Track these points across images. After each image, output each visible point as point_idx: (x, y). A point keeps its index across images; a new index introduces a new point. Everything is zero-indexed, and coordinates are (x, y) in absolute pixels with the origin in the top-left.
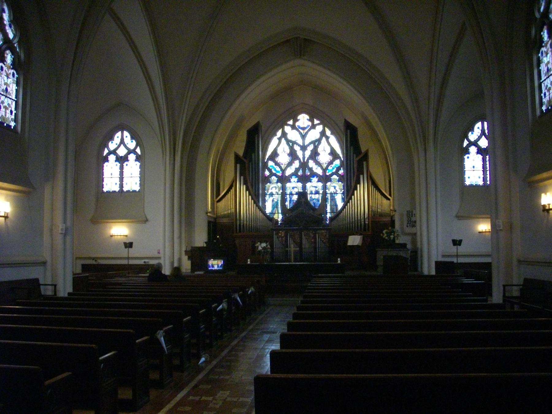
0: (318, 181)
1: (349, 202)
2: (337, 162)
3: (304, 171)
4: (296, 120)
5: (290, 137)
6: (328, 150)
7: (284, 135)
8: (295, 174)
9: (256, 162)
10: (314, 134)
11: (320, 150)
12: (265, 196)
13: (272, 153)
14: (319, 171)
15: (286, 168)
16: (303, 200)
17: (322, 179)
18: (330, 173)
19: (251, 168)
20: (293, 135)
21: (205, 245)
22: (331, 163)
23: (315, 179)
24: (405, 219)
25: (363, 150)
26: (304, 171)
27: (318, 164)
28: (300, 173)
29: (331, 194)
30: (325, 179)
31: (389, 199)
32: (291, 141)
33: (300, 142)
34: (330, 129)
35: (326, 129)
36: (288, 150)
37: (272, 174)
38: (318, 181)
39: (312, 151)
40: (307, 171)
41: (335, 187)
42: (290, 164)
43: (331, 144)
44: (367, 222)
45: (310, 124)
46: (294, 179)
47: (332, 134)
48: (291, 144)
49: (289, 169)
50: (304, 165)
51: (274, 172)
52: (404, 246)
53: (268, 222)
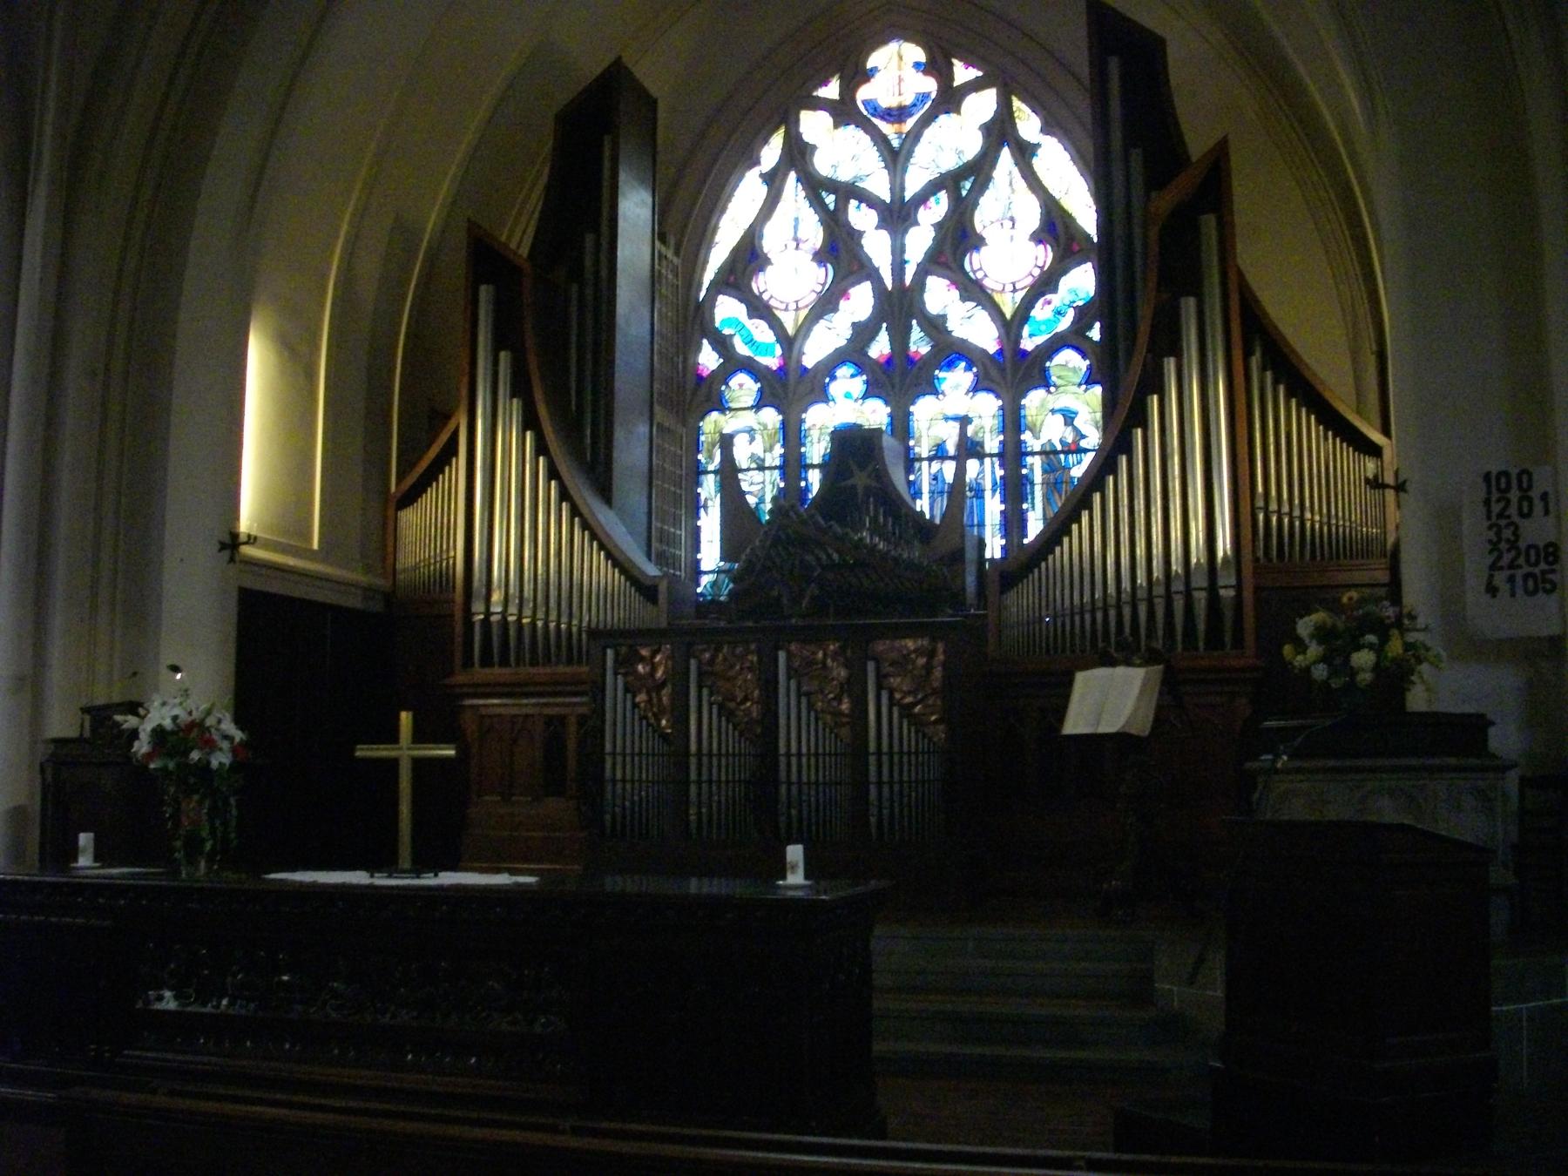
0: (976, 388)
1: (1114, 470)
2: (1081, 282)
3: (900, 338)
4: (857, 75)
5: (823, 164)
6: (1031, 215)
7: (798, 154)
8: (853, 353)
9: (604, 273)
10: (954, 139)
11: (984, 217)
12: (698, 484)
13: (736, 252)
14: (981, 332)
15: (806, 328)
16: (860, 480)
17: (994, 373)
18: (1040, 339)
19: (539, 306)
20: (840, 151)
22: (1046, 283)
23: (957, 380)
24: (1473, 527)
25: (1197, 144)
26: (900, 338)
27: (974, 291)
28: (880, 347)
29: (1048, 453)
30: (1012, 372)
31: (1375, 451)
32: (833, 186)
33: (880, 186)
34: (1037, 105)
35: (1017, 103)
36: (814, 234)
37: (733, 364)
38: (976, 388)
39: (938, 227)
40: (916, 333)
41: (1069, 417)
42: (827, 303)
43: (1046, 183)
44: (1227, 594)
45: (930, 85)
46: (847, 383)
47: (1046, 129)
48: (834, 199)
49: (820, 328)
50: (899, 306)
51: (742, 349)
52: (1466, 733)
53: (636, 599)
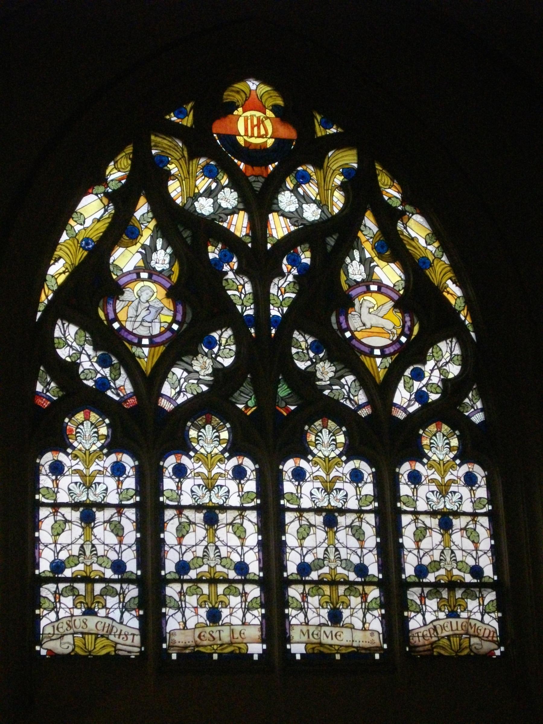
7: (149, 178)
20: (204, 192)
23: (326, 440)
48: (184, 229)
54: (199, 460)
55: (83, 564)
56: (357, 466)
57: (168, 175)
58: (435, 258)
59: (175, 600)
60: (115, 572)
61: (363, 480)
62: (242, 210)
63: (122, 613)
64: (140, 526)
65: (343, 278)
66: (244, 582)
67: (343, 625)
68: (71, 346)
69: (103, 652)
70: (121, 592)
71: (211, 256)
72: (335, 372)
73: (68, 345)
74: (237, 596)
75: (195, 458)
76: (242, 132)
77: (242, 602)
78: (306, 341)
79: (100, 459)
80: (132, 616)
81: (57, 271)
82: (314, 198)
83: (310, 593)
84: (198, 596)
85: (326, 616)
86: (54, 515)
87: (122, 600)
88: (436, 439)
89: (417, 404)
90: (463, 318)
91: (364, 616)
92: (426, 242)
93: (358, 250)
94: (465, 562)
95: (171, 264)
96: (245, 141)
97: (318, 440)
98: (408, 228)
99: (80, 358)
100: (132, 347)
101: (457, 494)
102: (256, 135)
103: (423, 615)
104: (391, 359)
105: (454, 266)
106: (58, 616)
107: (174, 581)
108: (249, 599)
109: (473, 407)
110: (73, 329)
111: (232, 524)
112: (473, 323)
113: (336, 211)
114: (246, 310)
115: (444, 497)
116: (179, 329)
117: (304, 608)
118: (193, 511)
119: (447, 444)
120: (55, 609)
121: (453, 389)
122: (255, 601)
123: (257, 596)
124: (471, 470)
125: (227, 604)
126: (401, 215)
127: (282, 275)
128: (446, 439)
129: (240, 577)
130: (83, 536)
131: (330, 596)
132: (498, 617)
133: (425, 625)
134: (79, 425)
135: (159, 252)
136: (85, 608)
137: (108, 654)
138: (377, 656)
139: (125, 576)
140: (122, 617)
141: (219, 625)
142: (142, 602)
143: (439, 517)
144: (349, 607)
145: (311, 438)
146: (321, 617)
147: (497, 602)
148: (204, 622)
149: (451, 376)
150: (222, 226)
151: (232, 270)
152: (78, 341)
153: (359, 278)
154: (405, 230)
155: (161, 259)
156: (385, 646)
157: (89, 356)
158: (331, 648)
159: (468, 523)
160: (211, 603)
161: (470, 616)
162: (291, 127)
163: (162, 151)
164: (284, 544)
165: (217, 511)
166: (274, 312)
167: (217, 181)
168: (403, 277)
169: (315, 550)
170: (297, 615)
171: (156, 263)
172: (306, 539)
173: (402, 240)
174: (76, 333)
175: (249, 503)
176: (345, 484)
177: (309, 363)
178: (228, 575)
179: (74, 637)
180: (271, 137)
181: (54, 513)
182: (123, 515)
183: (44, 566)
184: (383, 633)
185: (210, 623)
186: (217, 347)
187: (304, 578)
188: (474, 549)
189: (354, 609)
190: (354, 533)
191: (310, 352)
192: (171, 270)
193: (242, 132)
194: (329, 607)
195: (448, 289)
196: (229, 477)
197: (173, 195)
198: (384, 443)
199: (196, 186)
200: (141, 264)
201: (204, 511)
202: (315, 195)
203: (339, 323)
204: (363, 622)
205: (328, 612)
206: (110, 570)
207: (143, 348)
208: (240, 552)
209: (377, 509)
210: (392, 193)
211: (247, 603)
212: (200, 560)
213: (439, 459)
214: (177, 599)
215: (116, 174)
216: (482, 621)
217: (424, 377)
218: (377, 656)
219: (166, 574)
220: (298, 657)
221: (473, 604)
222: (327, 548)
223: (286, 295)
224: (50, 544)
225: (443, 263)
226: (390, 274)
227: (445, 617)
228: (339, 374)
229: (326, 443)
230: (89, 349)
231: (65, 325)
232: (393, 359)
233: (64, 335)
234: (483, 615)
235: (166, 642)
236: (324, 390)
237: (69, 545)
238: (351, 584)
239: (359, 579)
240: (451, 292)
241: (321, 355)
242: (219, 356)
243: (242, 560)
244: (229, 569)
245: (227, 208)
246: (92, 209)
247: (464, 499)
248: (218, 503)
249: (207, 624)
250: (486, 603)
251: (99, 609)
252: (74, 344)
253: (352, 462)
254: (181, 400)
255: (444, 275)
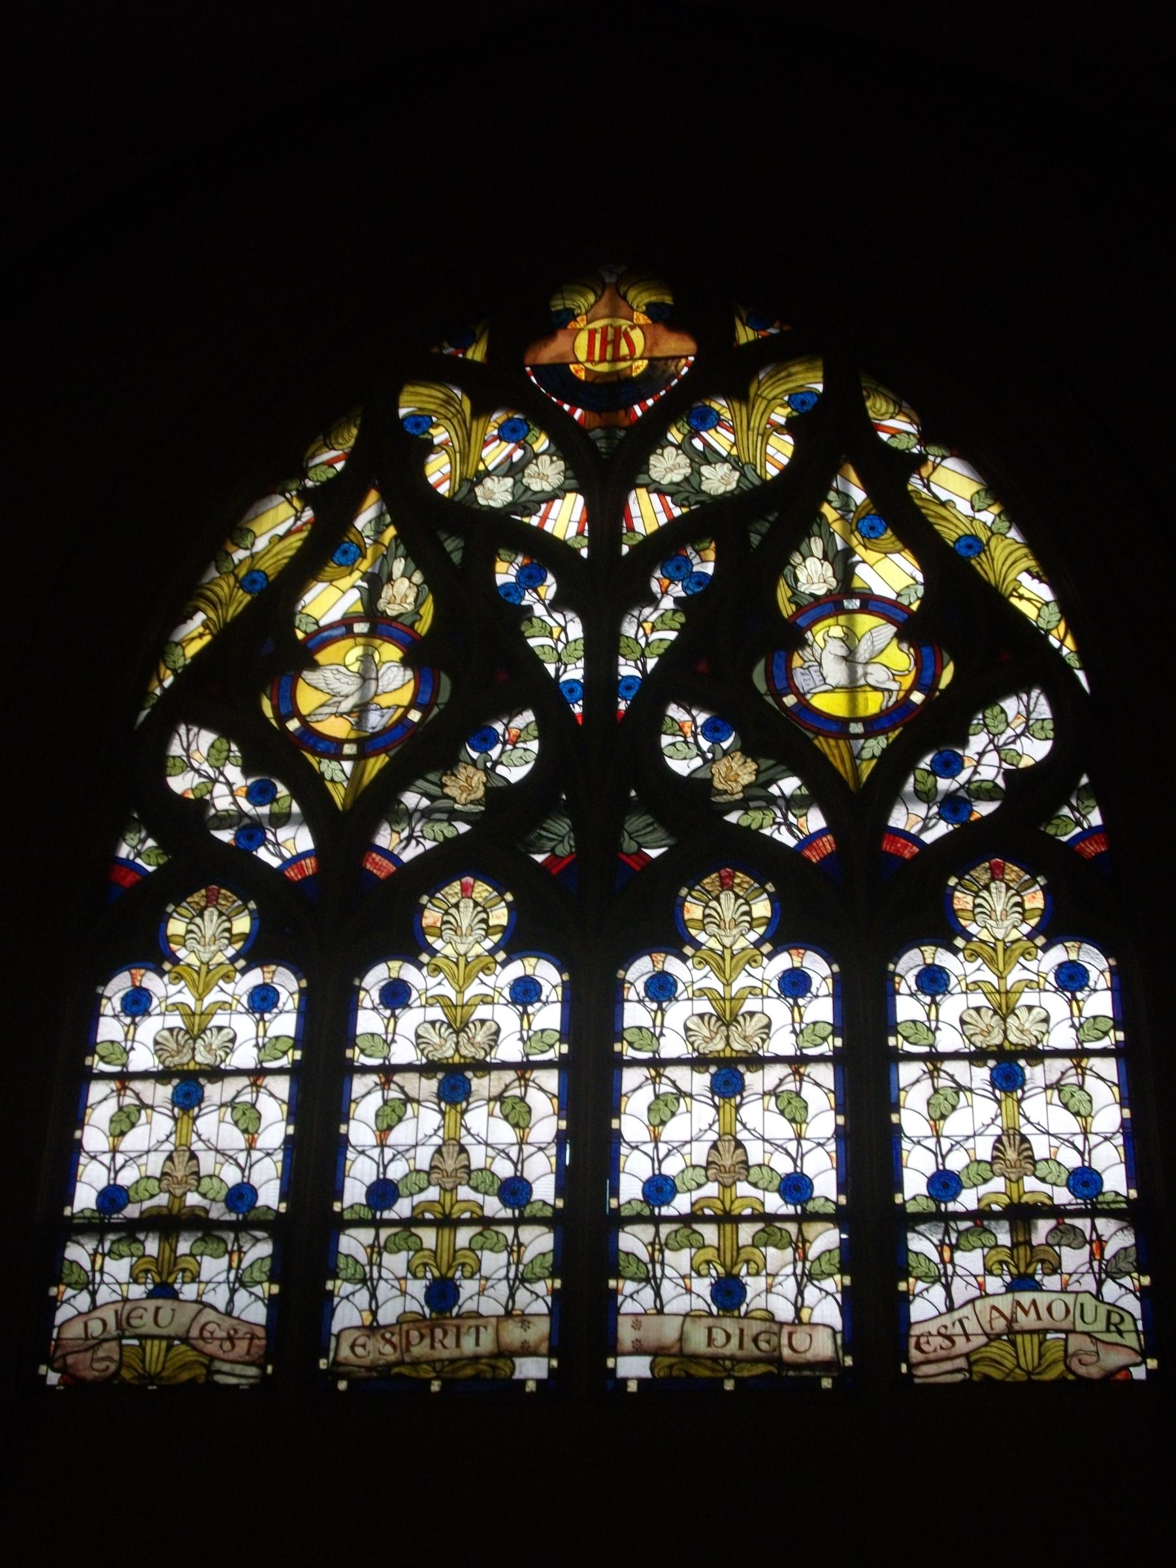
7: (392, 459)
8: (491, 845)
20: (479, 458)
21: (100, 990)
27: (784, 736)
48: (456, 540)
50: (600, 750)
54: (976, 955)
55: (438, 1188)
56: (529, 971)
57: (429, 447)
58: (993, 534)
59: (639, 1260)
60: (506, 1203)
61: (276, 1006)
62: (571, 491)
63: (233, 1292)
64: (296, 1111)
65: (783, 593)
66: (1093, 1213)
67: (747, 1313)
68: (197, 771)
69: (185, 1376)
70: (235, 1248)
71: (500, 580)
72: (758, 772)
73: (193, 768)
74: (782, 1248)
75: (173, 975)
76: (582, 355)
77: (509, 1264)
78: (694, 719)
79: (487, 972)
80: (253, 1297)
81: (194, 636)
82: (724, 454)
83: (671, 1241)
84: (135, 1259)
85: (706, 1292)
86: (119, 1095)
87: (235, 1264)
88: (989, 899)
89: (942, 823)
90: (1056, 644)
91: (800, 1292)
92: (973, 507)
93: (820, 537)
94: (218, 1177)
95: (418, 603)
96: (587, 370)
97: (191, 931)
98: (932, 485)
99: (211, 792)
100: (319, 763)
101: (225, 1031)
102: (608, 356)
103: (947, 1288)
104: (887, 739)
105: (1036, 544)
106: (93, 1301)
107: (638, 1219)
108: (527, 1257)
109: (1078, 823)
110: (207, 738)
111: (774, 1093)
112: (1082, 651)
113: (772, 472)
114: (565, 671)
115: (728, 1025)
116: (422, 719)
117: (371, 1278)
118: (964, 1064)
119: (1016, 904)
120: (88, 1285)
121: (1029, 791)
122: (539, 1262)
123: (832, 1246)
124: (268, 981)
125: (761, 1264)
126: (915, 463)
127: (654, 601)
128: (1013, 895)
129: (233, 1217)
130: (999, 1119)
131: (718, 1249)
132: (270, 1295)
133: (951, 1308)
134: (980, 890)
135: (397, 585)
136: (1011, 1274)
137: (193, 1380)
138: (826, 1383)
139: (528, 1211)
140: (231, 1301)
141: (451, 1317)
142: (563, 1262)
143: (992, 1063)
144: (478, 1276)
145: (431, 917)
146: (408, 1297)
147: (554, 1256)
148: (418, 1309)
149: (1025, 763)
150: (529, 525)
151: (541, 600)
152: (212, 761)
153: (821, 590)
154: (925, 490)
155: (403, 593)
156: (849, 1361)
157: (229, 784)
158: (716, 1367)
159: (781, 1080)
160: (438, 1268)
161: (1067, 1284)
162: (687, 338)
163: (420, 409)
164: (897, 1131)
165: (469, 1074)
166: (627, 669)
167: (522, 444)
168: (920, 577)
169: (688, 1146)
170: (353, 1293)
171: (389, 603)
172: (669, 1125)
173: (917, 509)
174: (212, 746)
175: (276, 1059)
176: (1043, 994)
177: (698, 762)
178: (763, 1204)
179: (121, 1346)
180: (641, 358)
181: (119, 1090)
182: (531, 1084)
183: (85, 1198)
184: (843, 1332)
185: (431, 1311)
186: (499, 747)
187: (943, 1207)
188: (1078, 1130)
189: (775, 1276)
190: (236, 1118)
191: (701, 739)
192: (417, 613)
193: (582, 355)
194: (429, 1275)
195: (1021, 591)
196: (240, 1008)
197: (432, 480)
198: (865, 912)
199: (482, 460)
200: (359, 608)
201: (440, 1076)
202: (728, 448)
203: (769, 677)
204: (795, 1305)
205: (426, 1287)
206: (776, 1196)
207: (343, 763)
208: (242, 1162)
209: (1122, 1045)
210: (897, 427)
211: (808, 1265)
212: (424, 1176)
213: (724, 946)
214: (363, 1259)
215: (329, 460)
216: (1098, 1296)
217: (962, 768)
218: (826, 1383)
219: (905, 1202)
220: (632, 1387)
221: (213, 1267)
222: (172, 1152)
223: (654, 636)
224: (645, 1143)
225: (1010, 541)
226: (892, 573)
227: (1003, 1290)
228: (763, 778)
229: (727, 920)
230: (233, 773)
231: (192, 734)
232: (891, 740)
233: (187, 750)
234: (1100, 1283)
235: (327, 1357)
236: (728, 812)
237: (968, 1137)
238: (486, 1222)
239: (507, 1213)
240: (1027, 595)
241: (725, 745)
242: (502, 763)
243: (1086, 1164)
244: (486, 1193)
245: (543, 491)
246: (277, 525)
247: (1052, 1024)
248: (473, 1058)
249: (424, 1316)
250: (244, 1265)
251: (184, 1283)
252: (205, 767)
253: (785, 955)
254: (407, 856)
255: (1013, 563)
